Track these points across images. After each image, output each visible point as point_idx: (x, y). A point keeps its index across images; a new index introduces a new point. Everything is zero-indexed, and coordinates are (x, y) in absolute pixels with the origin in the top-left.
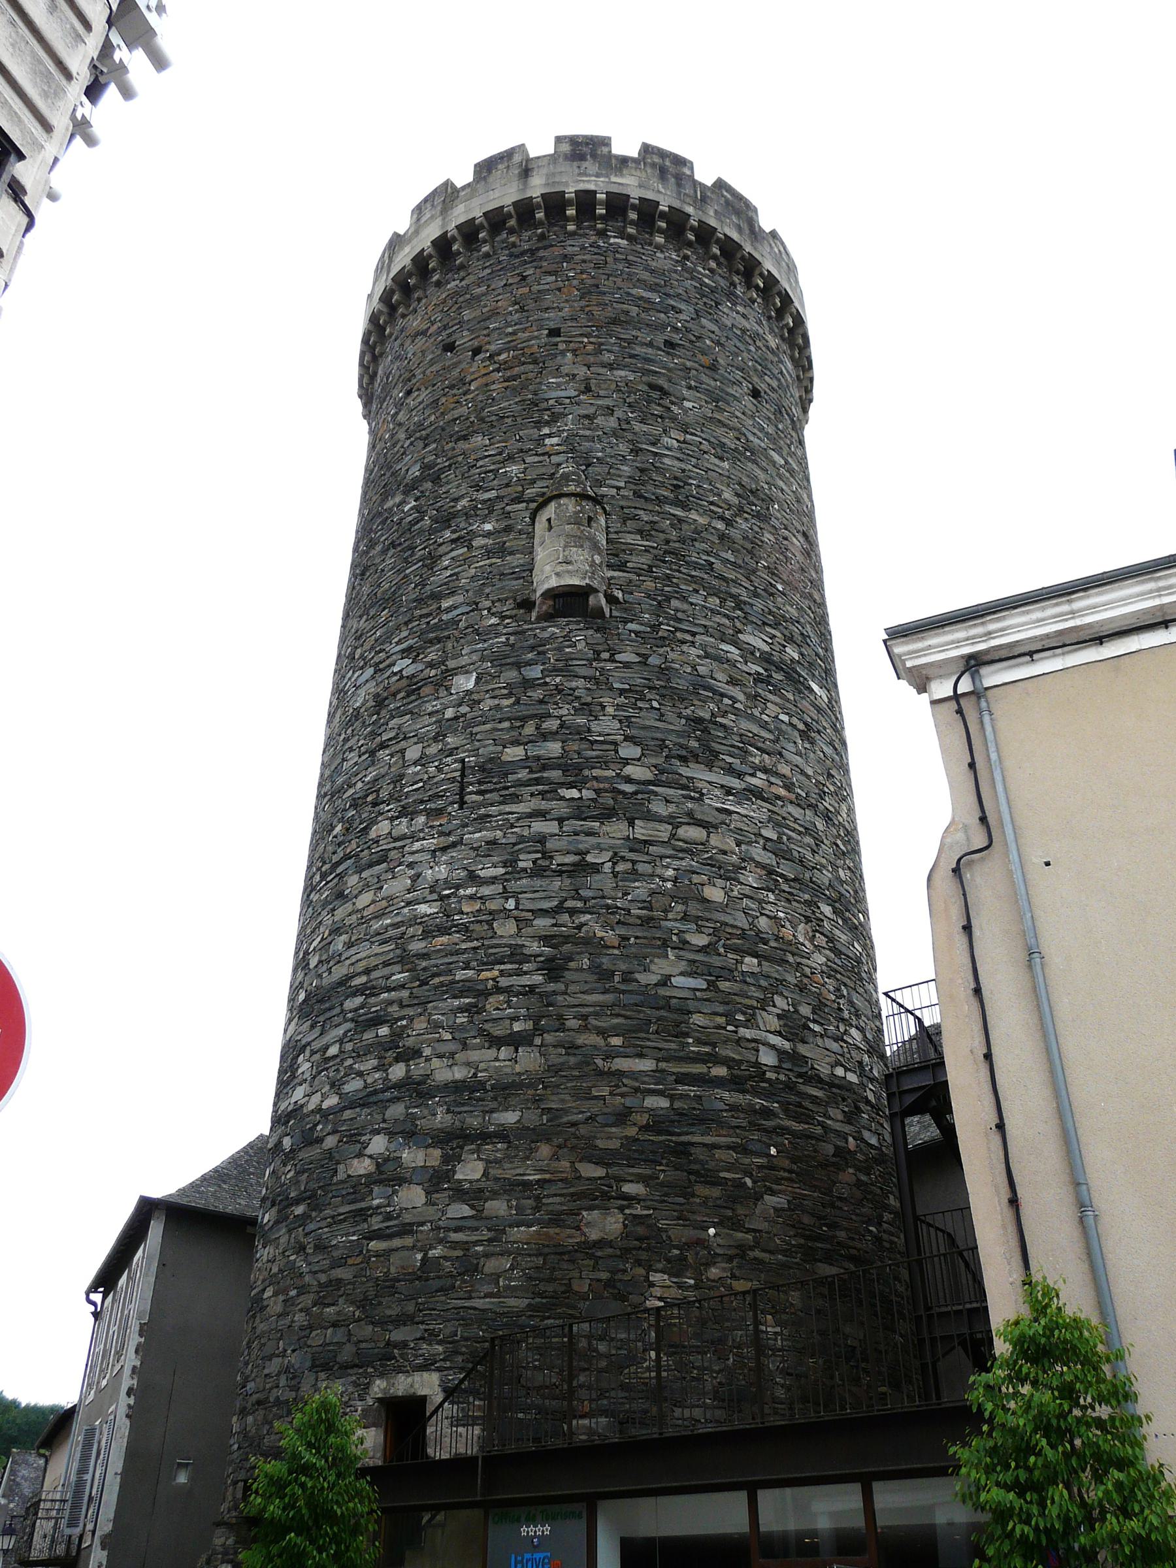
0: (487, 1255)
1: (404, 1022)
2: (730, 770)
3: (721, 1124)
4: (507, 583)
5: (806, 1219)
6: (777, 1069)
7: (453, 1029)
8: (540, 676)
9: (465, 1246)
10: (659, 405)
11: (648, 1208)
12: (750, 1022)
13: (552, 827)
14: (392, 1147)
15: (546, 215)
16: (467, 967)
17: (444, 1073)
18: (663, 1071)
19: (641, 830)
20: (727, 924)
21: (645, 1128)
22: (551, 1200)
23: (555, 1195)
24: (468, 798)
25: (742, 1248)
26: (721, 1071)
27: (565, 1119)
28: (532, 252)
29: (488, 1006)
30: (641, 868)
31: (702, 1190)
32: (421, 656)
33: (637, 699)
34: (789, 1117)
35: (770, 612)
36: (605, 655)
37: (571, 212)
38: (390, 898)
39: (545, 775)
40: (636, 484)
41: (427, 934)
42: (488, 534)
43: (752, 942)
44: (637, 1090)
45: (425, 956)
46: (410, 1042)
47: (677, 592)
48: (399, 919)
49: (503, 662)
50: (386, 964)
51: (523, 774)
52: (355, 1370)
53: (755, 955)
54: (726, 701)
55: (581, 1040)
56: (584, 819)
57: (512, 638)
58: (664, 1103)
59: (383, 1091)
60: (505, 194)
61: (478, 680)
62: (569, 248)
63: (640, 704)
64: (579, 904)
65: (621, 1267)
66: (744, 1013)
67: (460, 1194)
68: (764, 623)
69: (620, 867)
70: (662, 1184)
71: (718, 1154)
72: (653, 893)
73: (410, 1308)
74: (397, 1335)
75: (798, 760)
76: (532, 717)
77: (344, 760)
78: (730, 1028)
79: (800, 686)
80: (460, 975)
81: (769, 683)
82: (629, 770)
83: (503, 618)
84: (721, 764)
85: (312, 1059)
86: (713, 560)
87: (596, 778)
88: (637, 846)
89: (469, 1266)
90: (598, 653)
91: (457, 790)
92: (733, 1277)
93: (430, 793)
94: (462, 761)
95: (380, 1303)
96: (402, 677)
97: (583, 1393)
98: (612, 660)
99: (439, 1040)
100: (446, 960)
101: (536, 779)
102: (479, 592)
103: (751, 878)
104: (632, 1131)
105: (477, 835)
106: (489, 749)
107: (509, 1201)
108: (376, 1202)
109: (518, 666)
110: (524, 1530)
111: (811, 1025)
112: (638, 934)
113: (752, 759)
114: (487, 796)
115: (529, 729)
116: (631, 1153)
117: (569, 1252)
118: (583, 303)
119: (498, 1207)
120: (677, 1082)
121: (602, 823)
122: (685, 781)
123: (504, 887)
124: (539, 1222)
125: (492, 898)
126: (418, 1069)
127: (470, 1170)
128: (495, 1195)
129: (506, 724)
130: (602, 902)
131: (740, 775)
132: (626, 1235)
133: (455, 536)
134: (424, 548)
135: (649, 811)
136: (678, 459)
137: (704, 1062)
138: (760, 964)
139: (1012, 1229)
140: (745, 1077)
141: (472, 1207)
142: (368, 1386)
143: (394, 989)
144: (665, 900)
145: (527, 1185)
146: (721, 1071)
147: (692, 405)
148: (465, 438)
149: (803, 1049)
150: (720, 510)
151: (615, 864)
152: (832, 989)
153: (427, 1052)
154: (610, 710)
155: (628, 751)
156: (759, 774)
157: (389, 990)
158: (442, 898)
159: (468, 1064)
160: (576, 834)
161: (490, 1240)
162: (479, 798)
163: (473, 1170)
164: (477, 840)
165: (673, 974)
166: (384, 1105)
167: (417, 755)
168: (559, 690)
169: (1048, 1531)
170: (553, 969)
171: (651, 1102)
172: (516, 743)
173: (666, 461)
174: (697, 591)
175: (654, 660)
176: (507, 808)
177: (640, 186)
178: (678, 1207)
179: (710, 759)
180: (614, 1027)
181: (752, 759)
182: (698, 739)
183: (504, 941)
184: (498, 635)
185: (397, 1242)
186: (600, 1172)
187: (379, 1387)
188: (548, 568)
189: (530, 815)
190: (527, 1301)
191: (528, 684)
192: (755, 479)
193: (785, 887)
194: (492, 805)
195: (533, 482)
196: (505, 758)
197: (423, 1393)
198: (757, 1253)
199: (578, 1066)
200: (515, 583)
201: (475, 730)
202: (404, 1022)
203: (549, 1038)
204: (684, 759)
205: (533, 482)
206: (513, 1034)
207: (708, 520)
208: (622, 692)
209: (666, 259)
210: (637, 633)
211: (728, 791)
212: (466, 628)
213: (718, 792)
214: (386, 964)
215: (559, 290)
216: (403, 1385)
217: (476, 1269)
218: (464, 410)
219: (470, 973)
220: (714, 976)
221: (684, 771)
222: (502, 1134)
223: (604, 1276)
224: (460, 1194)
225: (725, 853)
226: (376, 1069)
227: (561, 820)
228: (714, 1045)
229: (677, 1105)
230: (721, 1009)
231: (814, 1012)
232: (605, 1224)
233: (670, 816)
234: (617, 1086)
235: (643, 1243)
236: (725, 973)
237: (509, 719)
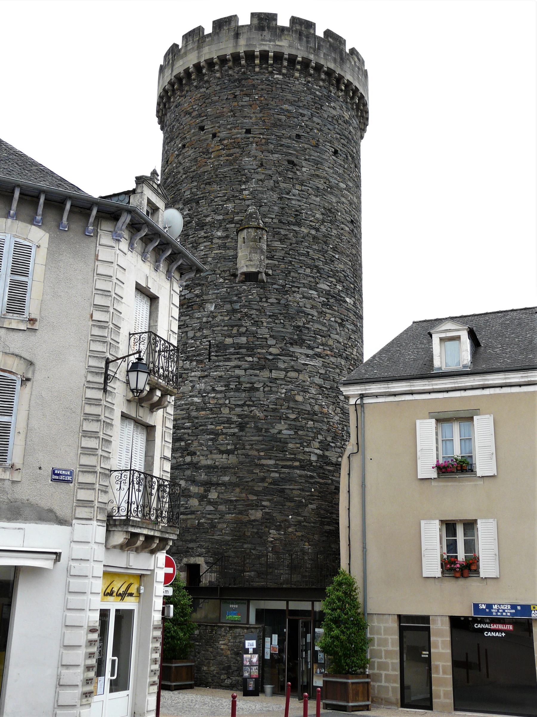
0: (219, 523)
1: (190, 442)
2: (310, 347)
3: (296, 482)
4: (227, 263)
5: (322, 512)
6: (316, 462)
7: (207, 446)
8: (239, 308)
9: (212, 519)
10: (292, 172)
11: (270, 510)
12: (308, 446)
13: (242, 372)
14: (187, 485)
15: (246, 61)
17: (204, 462)
18: (277, 464)
19: (274, 374)
20: (303, 410)
21: (270, 484)
22: (239, 506)
24: (211, 357)
25: (300, 522)
26: (297, 464)
27: (245, 480)
28: (240, 80)
30: (273, 389)
31: (288, 504)
32: (193, 291)
33: (275, 319)
34: (320, 478)
35: (332, 270)
37: (257, 61)
38: (183, 393)
40: (280, 216)
41: (197, 410)
42: (219, 238)
43: (312, 415)
44: (268, 471)
45: (197, 418)
46: (192, 449)
47: (293, 269)
48: (187, 402)
49: (225, 300)
50: (183, 419)
51: (232, 350)
53: (312, 420)
54: (310, 317)
55: (250, 453)
56: (254, 370)
57: (229, 290)
58: (277, 475)
59: (183, 465)
60: (227, 47)
61: (216, 307)
62: (256, 81)
63: (276, 321)
64: (251, 403)
66: (307, 442)
67: (210, 503)
68: (328, 276)
69: (266, 389)
70: (275, 502)
71: (294, 492)
72: (277, 399)
73: (194, 537)
74: (191, 545)
75: (337, 337)
76: (236, 326)
78: (301, 448)
79: (341, 301)
80: (210, 427)
81: (328, 305)
82: (271, 350)
83: (225, 280)
84: (305, 345)
86: (309, 250)
87: (259, 353)
88: (272, 381)
89: (213, 526)
90: (261, 298)
91: (208, 354)
92: (296, 531)
93: (198, 353)
94: (210, 341)
95: (184, 535)
96: (185, 298)
97: (247, 565)
98: (267, 302)
99: (202, 450)
100: (204, 421)
101: (237, 352)
102: (216, 266)
103: (313, 391)
104: (266, 485)
105: (215, 373)
106: (220, 338)
109: (231, 303)
110: (231, 606)
111: (331, 444)
113: (318, 341)
114: (219, 358)
115: (235, 331)
116: (266, 491)
118: (261, 115)
119: (222, 508)
120: (282, 468)
122: (291, 353)
124: (235, 513)
125: (220, 398)
126: (195, 459)
127: (213, 495)
128: (221, 504)
129: (226, 328)
131: (312, 348)
132: (263, 518)
133: (206, 235)
134: (193, 237)
135: (277, 366)
137: (291, 460)
138: (314, 424)
139: (348, 551)
140: (305, 465)
141: (214, 507)
142: (181, 560)
143: (186, 429)
144: (281, 401)
145: (231, 501)
146: (297, 464)
147: (306, 169)
148: (209, 184)
149: (327, 453)
150: (314, 224)
151: (264, 388)
152: (340, 429)
153: (198, 453)
154: (265, 324)
155: (271, 342)
156: (320, 347)
157: (184, 429)
158: (203, 396)
159: (213, 459)
160: (251, 375)
161: (220, 518)
162: (216, 358)
164: (215, 375)
165: (282, 429)
166: (184, 470)
167: (192, 335)
168: (246, 314)
169: (335, 617)
170: (242, 427)
171: (273, 475)
172: (230, 336)
173: (293, 202)
174: (301, 267)
175: (283, 302)
176: (227, 364)
177: (290, 46)
179: (301, 342)
180: (263, 448)
181: (318, 341)
182: (298, 335)
183: (225, 416)
184: (223, 288)
185: (189, 516)
187: (185, 560)
188: (243, 262)
189: (235, 367)
191: (234, 311)
192: (330, 203)
193: (326, 392)
194: (220, 361)
195: (238, 213)
196: (226, 343)
198: (305, 524)
199: (249, 462)
200: (230, 263)
201: (214, 329)
202: (190, 442)
203: (239, 452)
204: (291, 344)
205: (238, 213)
206: (227, 450)
207: (308, 230)
208: (270, 316)
210: (277, 289)
211: (307, 356)
212: (211, 282)
213: (303, 357)
214: (183, 419)
215: (251, 106)
216: (192, 560)
217: (215, 527)
218: (208, 168)
219: (213, 427)
220: (296, 429)
221: (291, 349)
222: (224, 484)
223: (255, 530)
224: (210, 503)
225: (304, 382)
226: (181, 457)
228: (295, 455)
229: (281, 476)
230: (298, 442)
231: (332, 439)
232: (257, 515)
233: (285, 368)
234: (262, 469)
235: (268, 520)
236: (301, 428)
237: (227, 326)
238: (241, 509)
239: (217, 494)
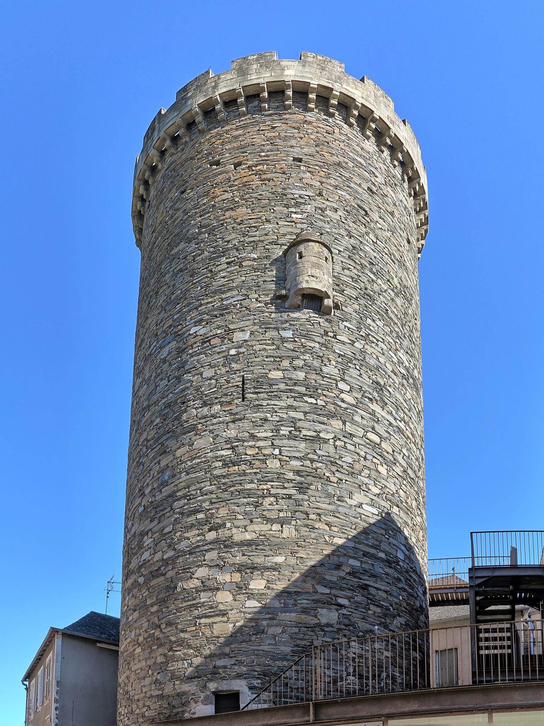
16: (252, 482)
22: (301, 602)
23: (304, 599)
24: (248, 396)
29: (264, 503)
30: (348, 446)
36: (331, 334)
39: (295, 388)
41: (225, 465)
51: (282, 386)
52: (197, 679)
58: (358, 564)
64: (316, 457)
65: (337, 637)
77: (156, 387)
80: (249, 486)
82: (343, 396)
85: (153, 537)
94: (243, 376)
101: (290, 390)
104: (343, 574)
107: (280, 600)
108: (202, 600)
112: (348, 479)
115: (286, 363)
117: (311, 627)
121: (328, 419)
122: (371, 411)
123: (272, 443)
126: (223, 533)
130: (328, 459)
136: (373, 250)
153: (228, 525)
154: (333, 363)
163: (259, 584)
171: (352, 562)
173: (366, 248)
178: (362, 614)
186: (327, 591)
187: (212, 686)
190: (291, 648)
191: (283, 340)
197: (237, 689)
209: (370, 145)
216: (225, 686)
227: (305, 413)
229: (363, 566)
238: (306, 605)
239: (264, 582)
